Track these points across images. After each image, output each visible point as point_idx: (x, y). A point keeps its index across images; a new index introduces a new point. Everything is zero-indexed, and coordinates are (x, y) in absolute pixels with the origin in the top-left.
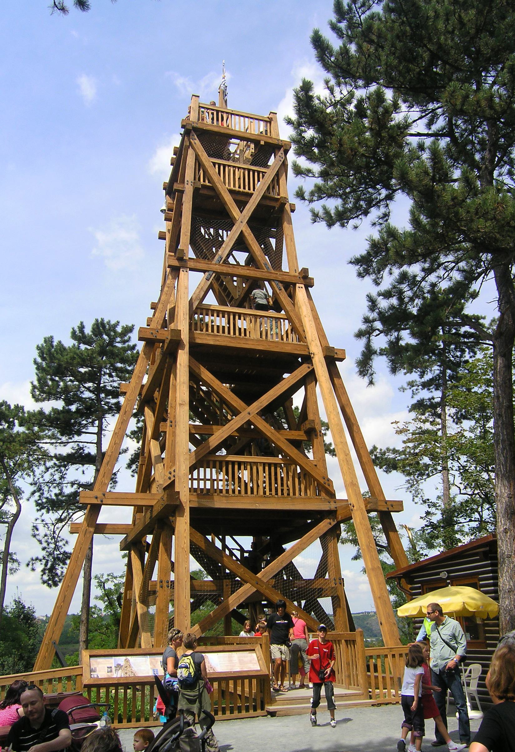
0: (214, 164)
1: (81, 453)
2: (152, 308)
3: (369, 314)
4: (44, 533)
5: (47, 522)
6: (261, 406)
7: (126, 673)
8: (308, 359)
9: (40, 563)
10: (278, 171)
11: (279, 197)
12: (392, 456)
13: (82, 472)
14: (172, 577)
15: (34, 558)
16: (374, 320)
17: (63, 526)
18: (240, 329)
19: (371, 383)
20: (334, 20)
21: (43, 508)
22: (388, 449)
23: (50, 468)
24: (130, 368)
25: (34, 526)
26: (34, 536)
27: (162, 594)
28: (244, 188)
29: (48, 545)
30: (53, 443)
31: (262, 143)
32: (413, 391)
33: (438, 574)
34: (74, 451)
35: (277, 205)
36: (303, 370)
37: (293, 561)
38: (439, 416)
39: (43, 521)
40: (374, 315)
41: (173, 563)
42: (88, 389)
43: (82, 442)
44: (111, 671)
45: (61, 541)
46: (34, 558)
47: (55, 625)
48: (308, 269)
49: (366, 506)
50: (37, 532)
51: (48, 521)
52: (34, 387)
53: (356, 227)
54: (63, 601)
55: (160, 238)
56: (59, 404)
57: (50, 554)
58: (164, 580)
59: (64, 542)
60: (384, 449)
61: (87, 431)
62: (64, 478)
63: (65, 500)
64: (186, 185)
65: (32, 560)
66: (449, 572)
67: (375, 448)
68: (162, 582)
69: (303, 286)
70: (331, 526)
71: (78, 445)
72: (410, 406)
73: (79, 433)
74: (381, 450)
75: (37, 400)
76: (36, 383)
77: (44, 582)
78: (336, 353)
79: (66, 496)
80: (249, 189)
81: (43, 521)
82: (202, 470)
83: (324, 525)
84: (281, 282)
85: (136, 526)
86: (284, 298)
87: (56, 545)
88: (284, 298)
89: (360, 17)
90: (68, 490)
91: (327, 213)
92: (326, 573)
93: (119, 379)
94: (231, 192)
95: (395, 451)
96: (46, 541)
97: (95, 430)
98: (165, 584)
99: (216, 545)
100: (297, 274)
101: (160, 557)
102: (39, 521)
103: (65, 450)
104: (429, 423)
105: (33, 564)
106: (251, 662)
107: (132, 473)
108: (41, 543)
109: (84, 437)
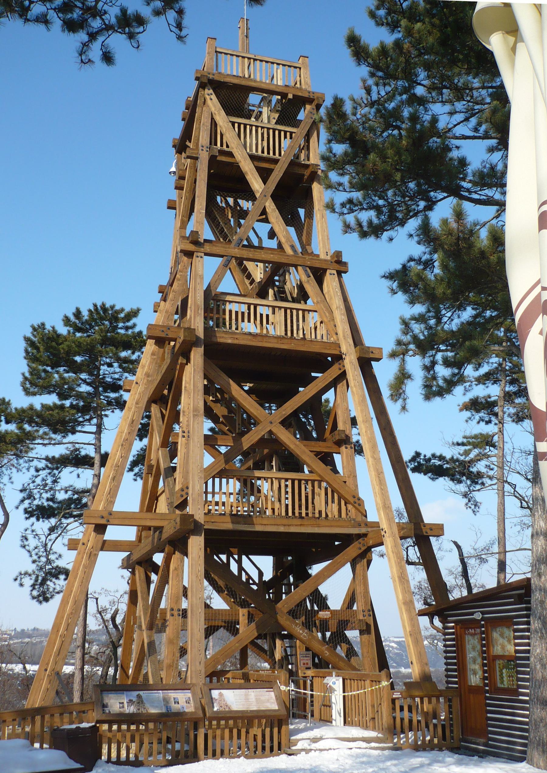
0: (233, 124)
1: (77, 455)
2: (160, 292)
3: (403, 337)
4: (35, 545)
5: (38, 533)
6: (285, 414)
7: (139, 709)
8: (339, 358)
9: (29, 578)
10: (308, 131)
11: (307, 163)
12: (437, 463)
13: (76, 476)
14: (184, 604)
15: (23, 573)
16: (409, 343)
17: (57, 538)
18: (261, 315)
19: (404, 408)
20: (373, 8)
21: (32, 516)
22: (434, 456)
23: (41, 470)
24: (134, 357)
25: (23, 536)
26: (24, 547)
27: (173, 623)
28: (269, 153)
29: (39, 557)
30: (47, 444)
31: (290, 96)
32: (465, 387)
33: (472, 614)
34: (68, 452)
35: (307, 173)
36: (333, 372)
37: (319, 588)
38: (496, 415)
39: (33, 531)
40: (407, 338)
41: (185, 589)
42: (84, 381)
43: (78, 443)
44: (123, 707)
45: (53, 553)
46: (23, 573)
47: (58, 655)
48: (341, 252)
49: (399, 532)
50: (26, 543)
51: (39, 532)
52: (26, 378)
53: (391, 239)
54: (67, 630)
55: (169, 208)
56: (51, 399)
57: (41, 569)
58: (175, 608)
59: (56, 556)
60: (429, 455)
61: (83, 430)
62: (57, 482)
63: (58, 507)
64: (200, 151)
65: (21, 574)
66: (483, 613)
67: (418, 454)
68: (172, 610)
69: (335, 272)
70: (361, 551)
71: (74, 446)
72: (461, 404)
73: (74, 432)
74: (425, 456)
75: (27, 392)
76: (27, 375)
77: (34, 598)
78: (372, 352)
79: (59, 503)
80: (274, 154)
81: (33, 531)
82: (217, 480)
83: (353, 550)
84: (310, 268)
85: (142, 545)
86: (311, 287)
87: (48, 559)
88: (311, 287)
89: (401, 4)
90: (61, 496)
91: (360, 225)
92: (353, 604)
93: (121, 370)
94: (253, 158)
95: (441, 458)
96: (37, 554)
97: (94, 429)
98: (176, 613)
99: (231, 568)
100: (328, 258)
101: (170, 582)
102: (29, 532)
103: (57, 451)
104: (484, 423)
105: (21, 578)
106: (268, 701)
107: (135, 477)
108: (31, 556)
109: (78, 437)
